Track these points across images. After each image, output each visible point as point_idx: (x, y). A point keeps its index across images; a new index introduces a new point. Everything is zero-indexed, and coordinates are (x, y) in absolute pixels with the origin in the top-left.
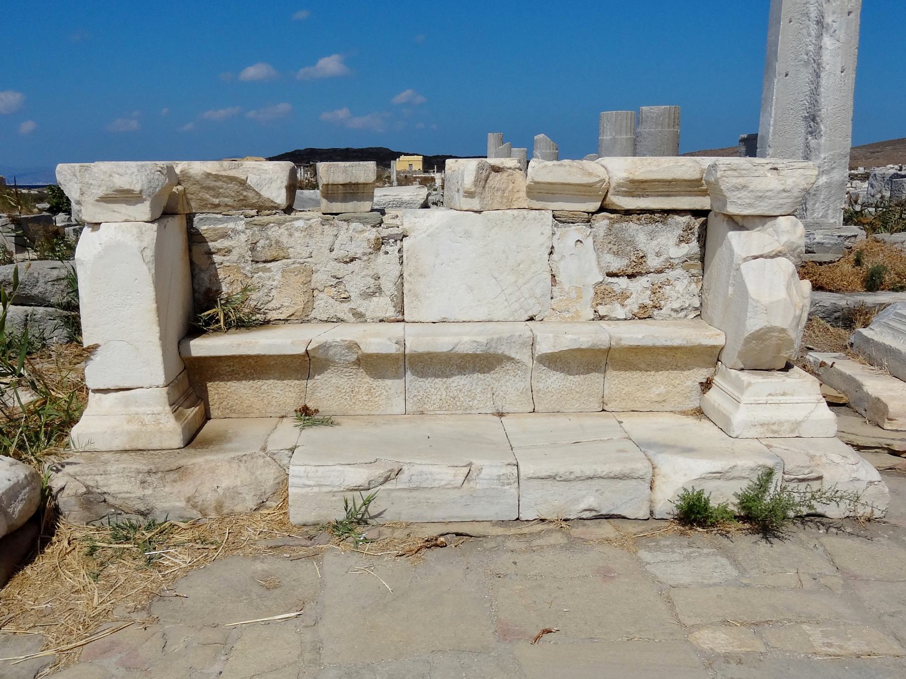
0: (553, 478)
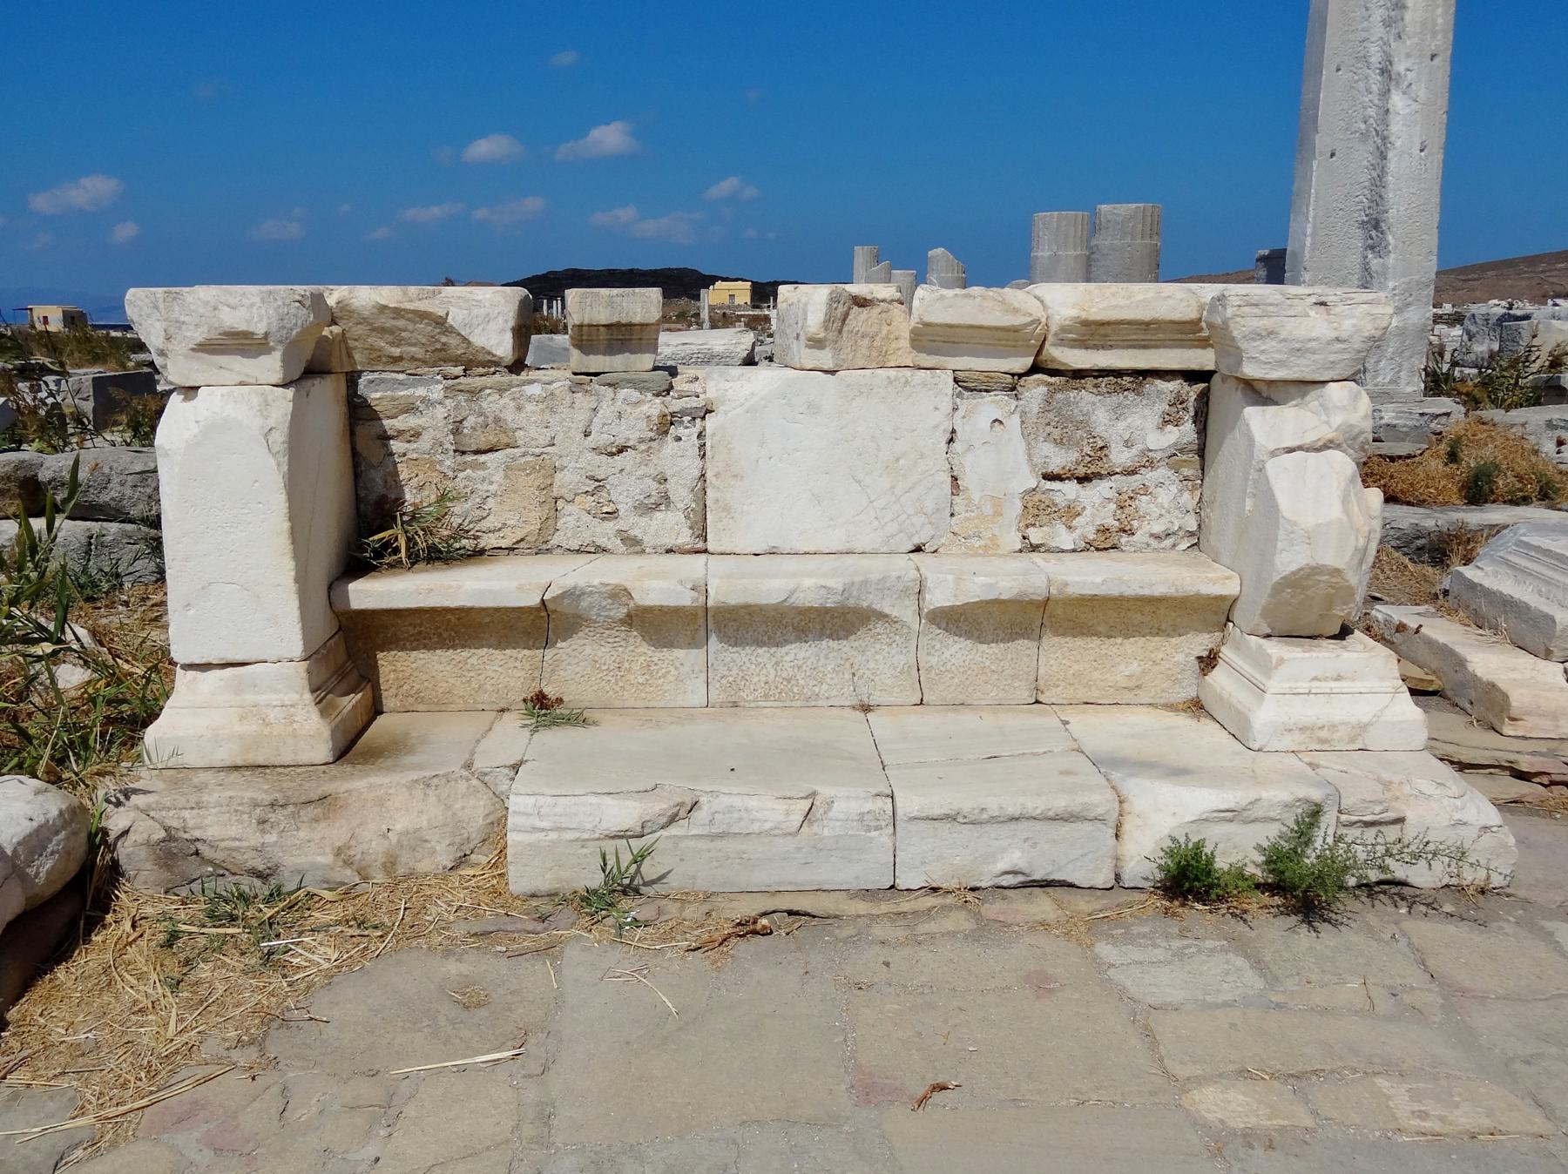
0: (951, 818)
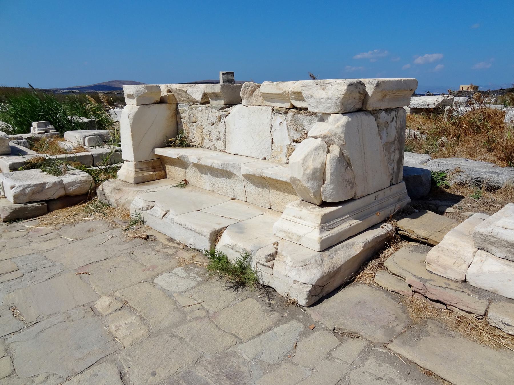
0: (181, 225)
